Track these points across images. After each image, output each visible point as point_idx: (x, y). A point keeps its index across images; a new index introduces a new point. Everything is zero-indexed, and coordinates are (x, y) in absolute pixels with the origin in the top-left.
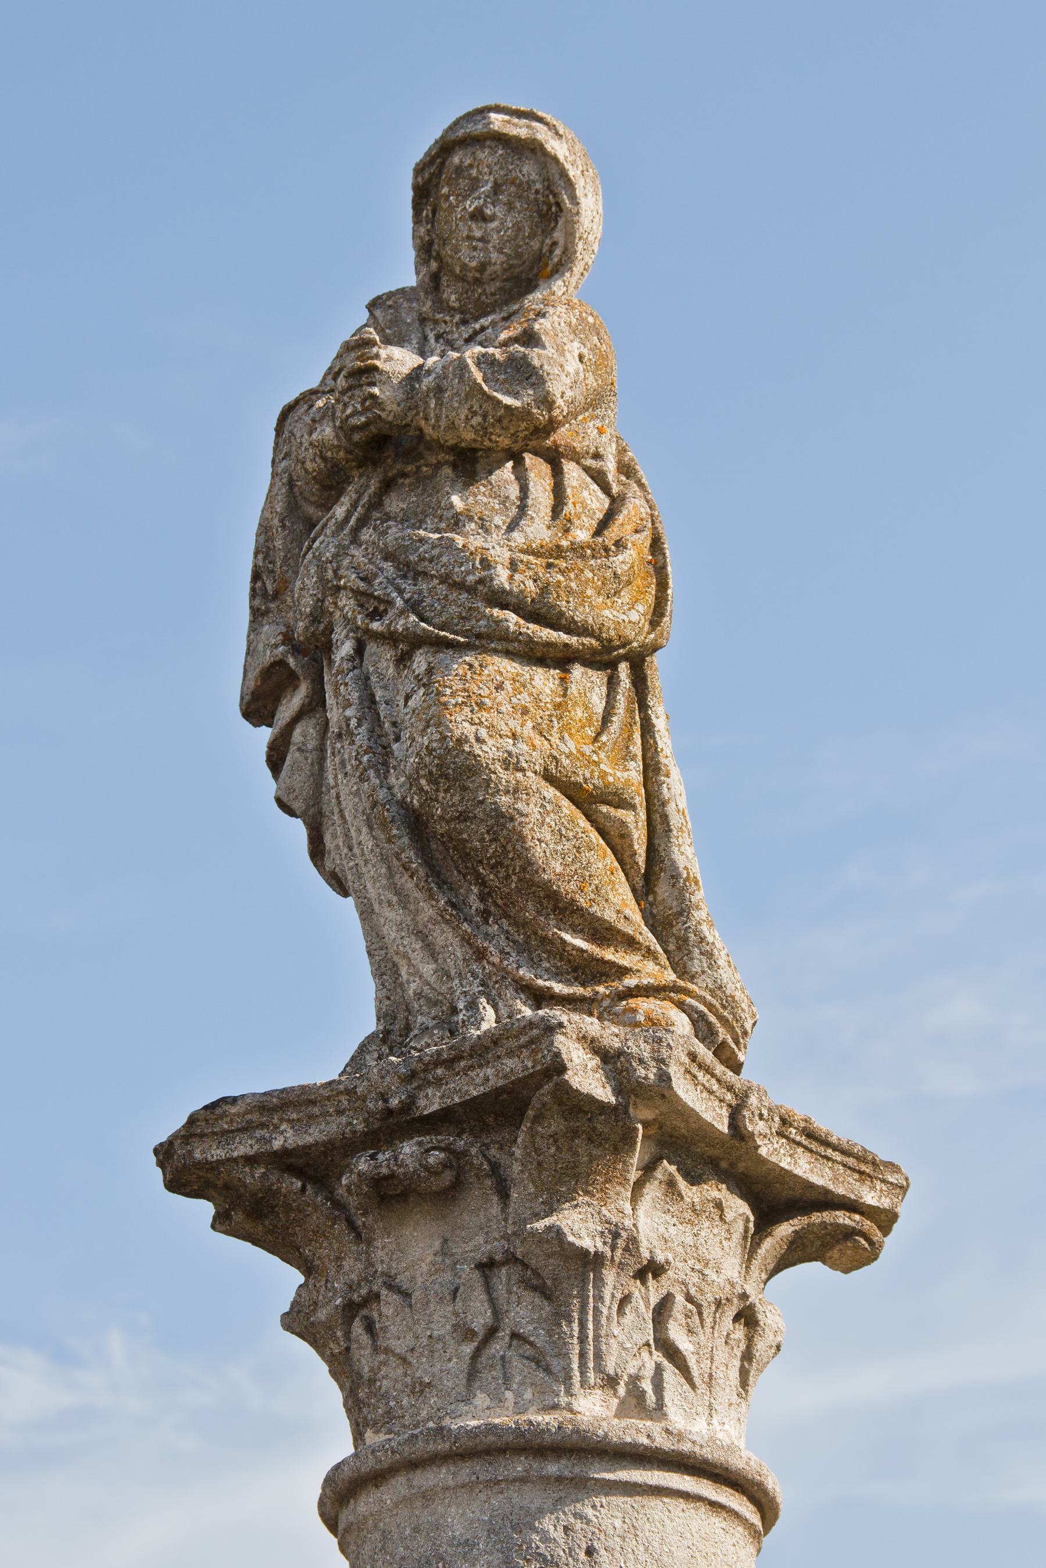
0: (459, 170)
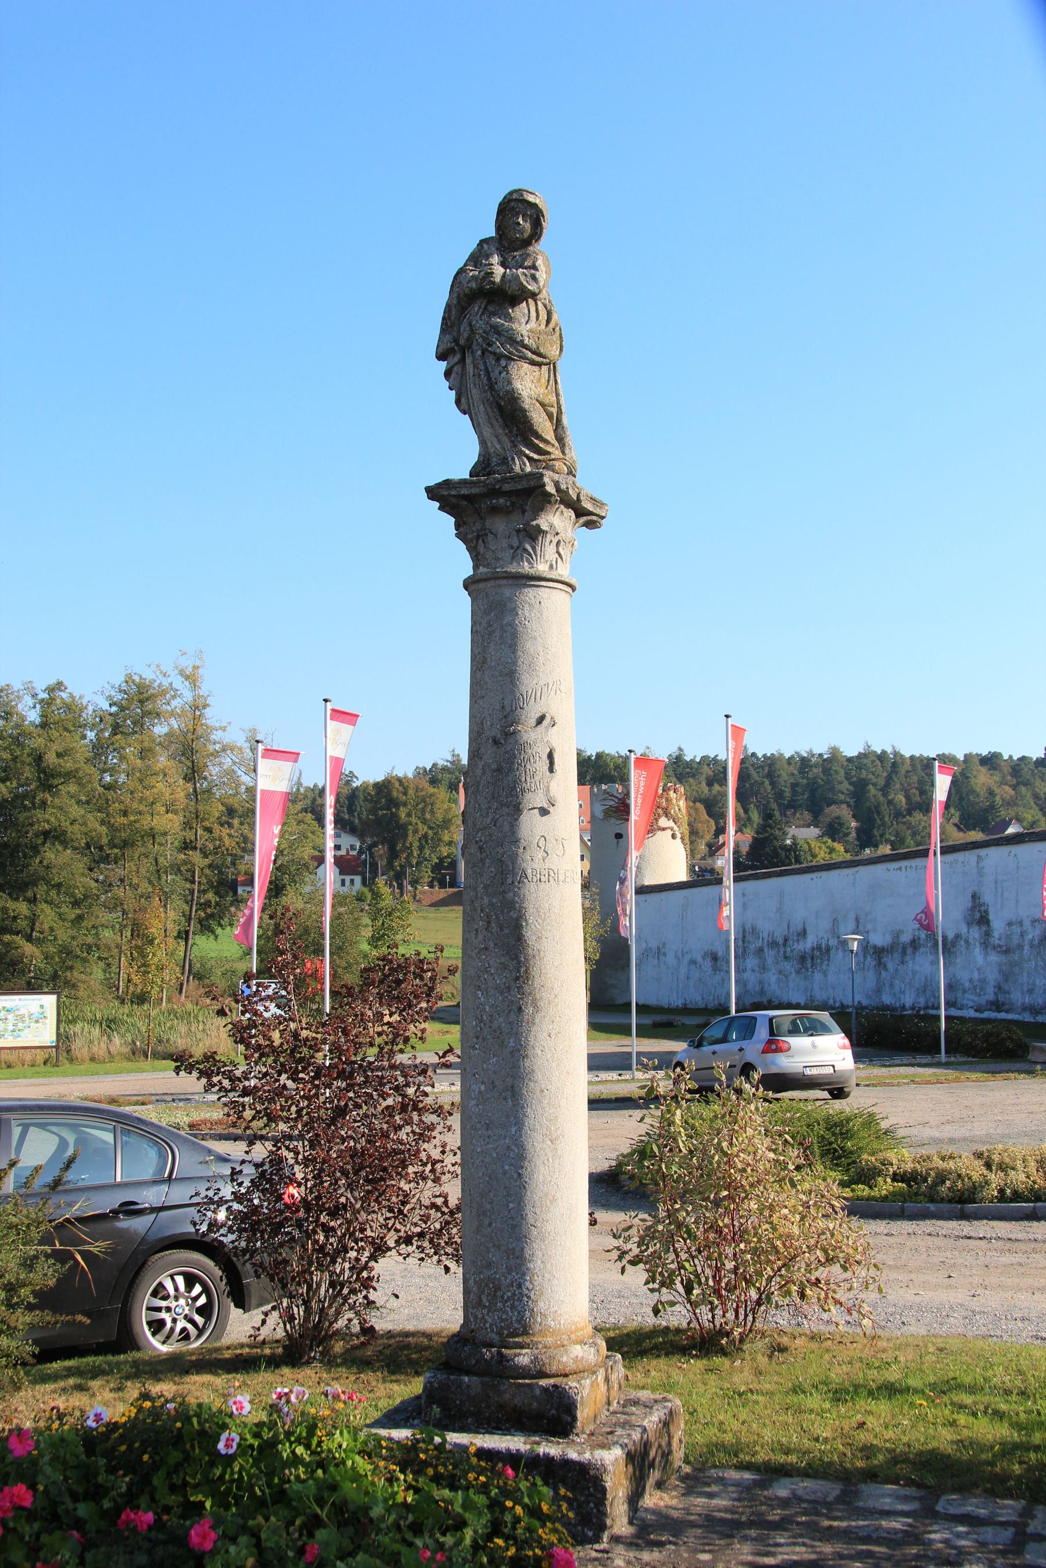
0: (513, 208)
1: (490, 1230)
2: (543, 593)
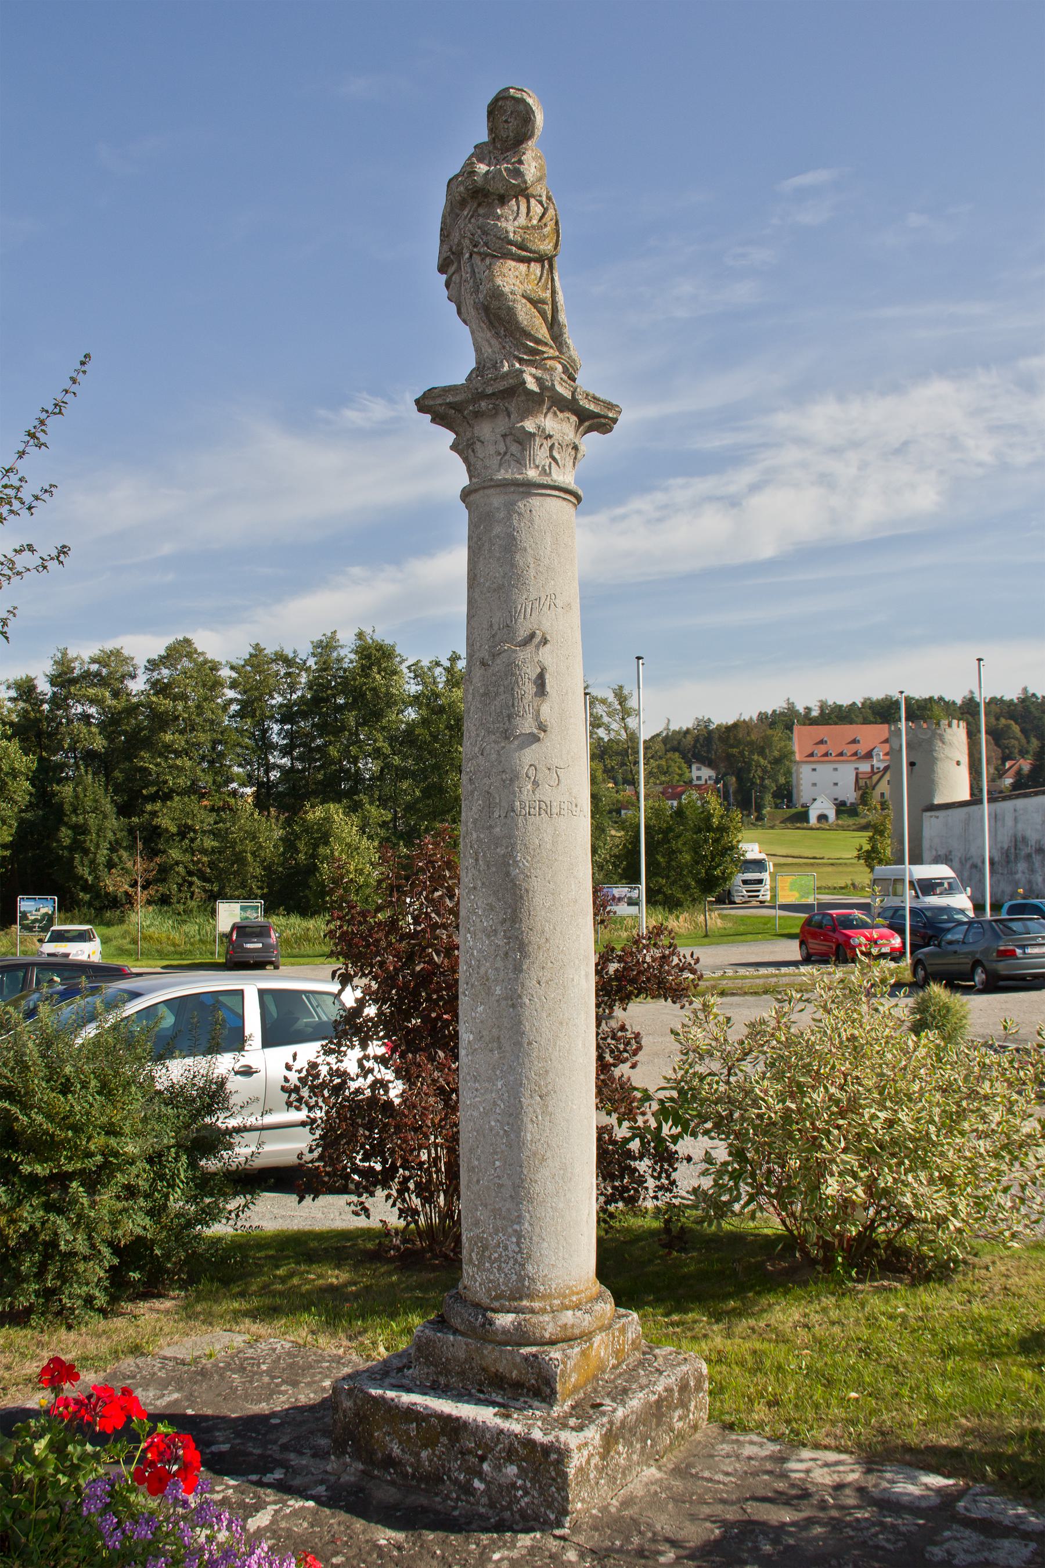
1: (478, 1187)
2: (535, 502)
